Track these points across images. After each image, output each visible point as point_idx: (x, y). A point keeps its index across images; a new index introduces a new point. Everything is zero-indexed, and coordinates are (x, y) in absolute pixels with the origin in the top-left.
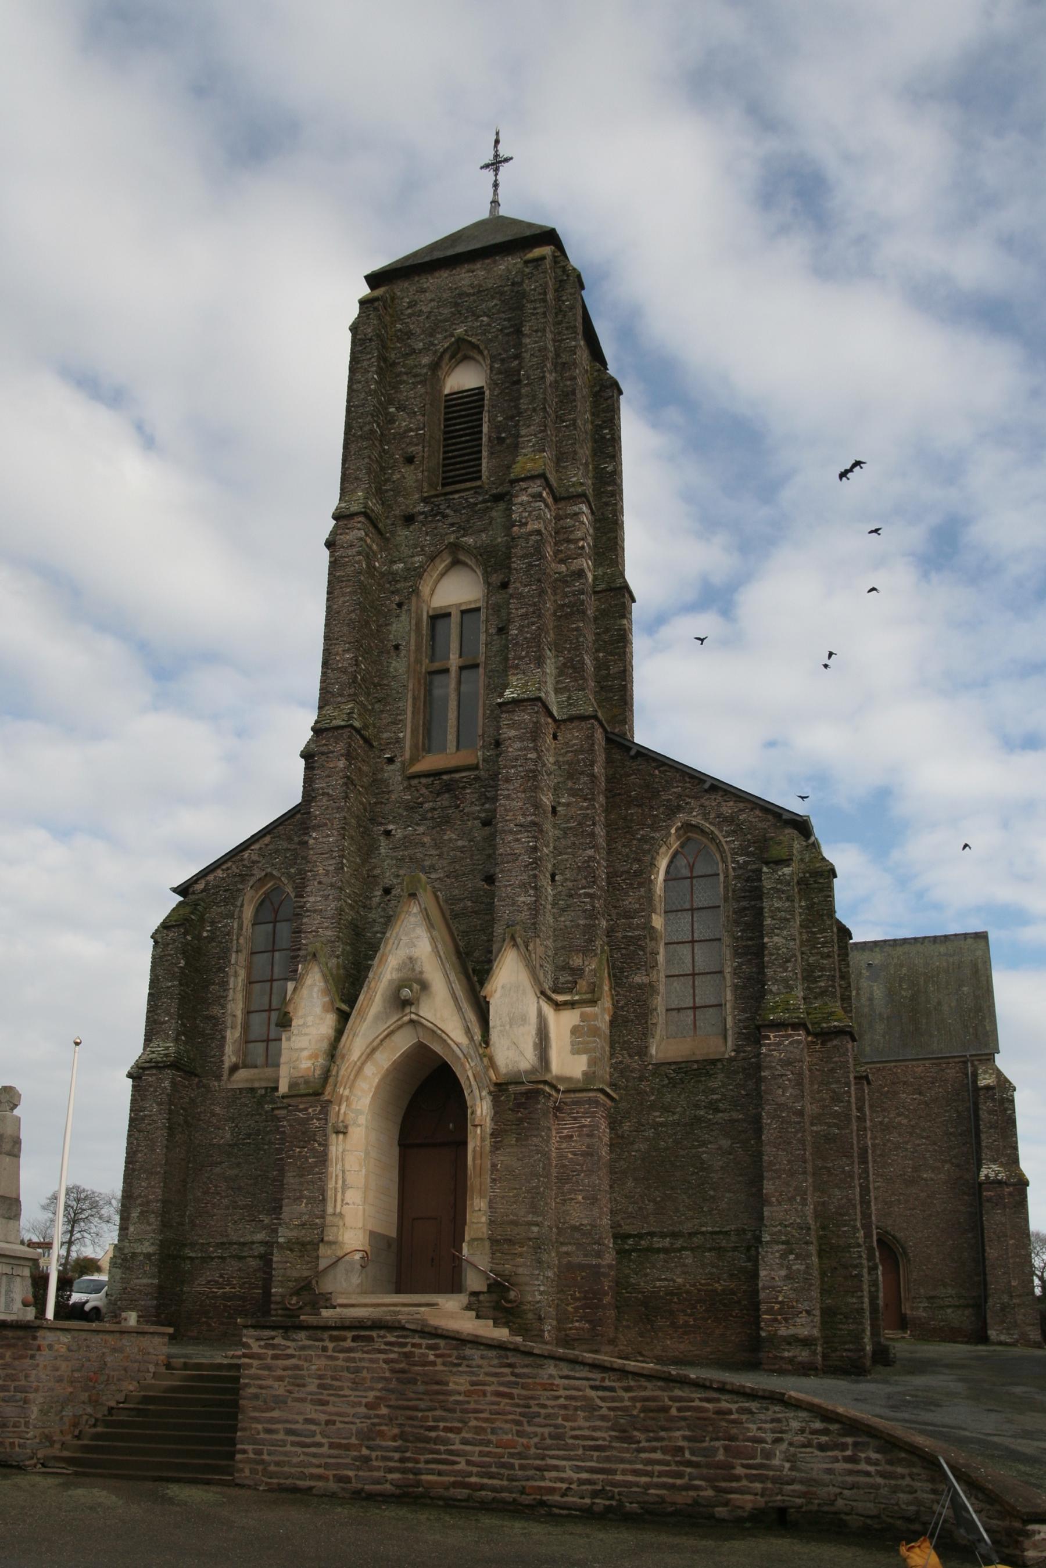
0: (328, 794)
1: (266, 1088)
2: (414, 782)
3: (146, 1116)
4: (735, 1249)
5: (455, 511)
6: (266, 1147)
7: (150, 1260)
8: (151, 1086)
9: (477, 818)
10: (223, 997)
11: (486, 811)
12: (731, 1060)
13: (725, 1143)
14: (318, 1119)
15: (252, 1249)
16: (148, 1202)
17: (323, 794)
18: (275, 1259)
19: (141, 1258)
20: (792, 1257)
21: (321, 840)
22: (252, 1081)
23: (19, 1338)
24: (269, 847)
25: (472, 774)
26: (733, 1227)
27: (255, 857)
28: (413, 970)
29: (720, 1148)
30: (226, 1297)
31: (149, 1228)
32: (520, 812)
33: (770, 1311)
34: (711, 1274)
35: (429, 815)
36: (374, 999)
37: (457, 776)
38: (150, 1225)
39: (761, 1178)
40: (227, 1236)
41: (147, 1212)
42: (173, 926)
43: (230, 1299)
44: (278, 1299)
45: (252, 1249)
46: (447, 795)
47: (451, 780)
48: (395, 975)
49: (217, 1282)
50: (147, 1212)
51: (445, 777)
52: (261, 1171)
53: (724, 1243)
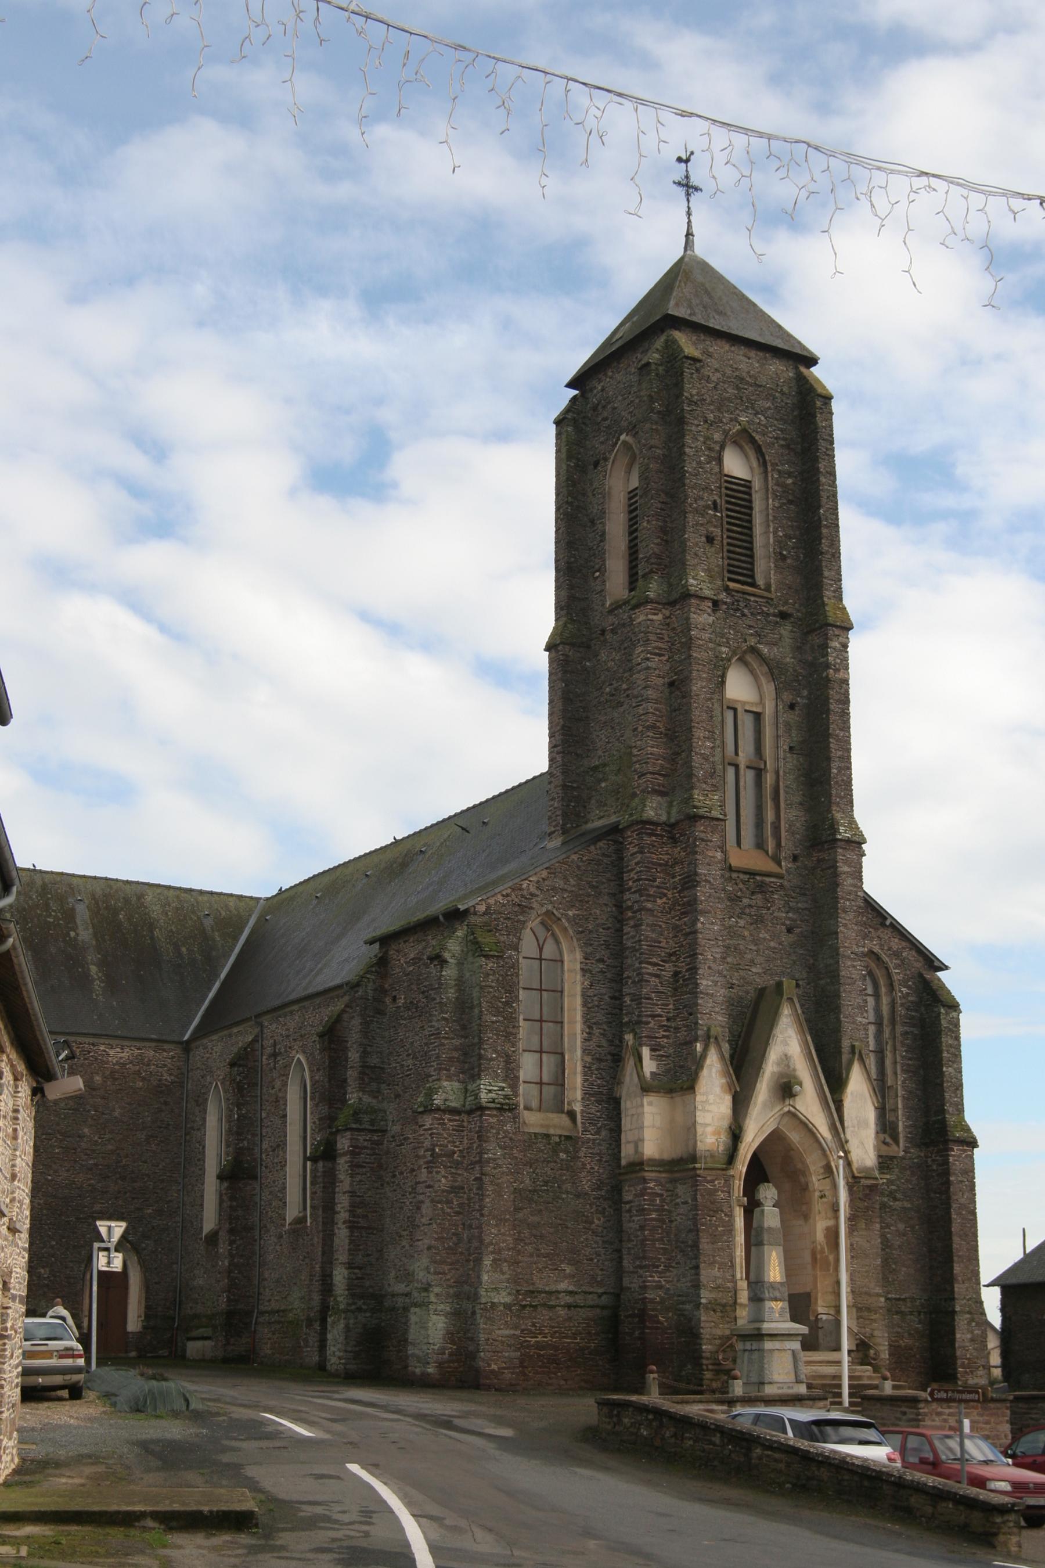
0: (710, 882)
1: (560, 1136)
2: (734, 875)
3: (490, 1158)
4: (911, 1313)
5: (752, 614)
6: (564, 1196)
7: (510, 1310)
8: (492, 1127)
9: (783, 924)
10: (512, 1034)
11: (790, 919)
12: (903, 1158)
13: (901, 1226)
14: (723, 1192)
15: (558, 1298)
16: (499, 1251)
17: (706, 881)
18: (703, 1319)
19: (502, 1308)
20: (974, 1324)
21: (707, 926)
22: (548, 1126)
23: (998, 1409)
24: (546, 883)
25: (778, 881)
26: (907, 1295)
27: (533, 889)
28: (789, 1067)
29: (897, 1231)
30: (539, 1346)
31: (503, 1277)
32: (854, 942)
33: (963, 1366)
34: (897, 1332)
35: (747, 911)
36: (763, 1090)
37: (768, 879)
38: (504, 1274)
39: (952, 1261)
40: (533, 1284)
41: (499, 1260)
42: (493, 956)
43: (543, 1348)
44: (708, 1355)
45: (558, 1298)
46: (760, 896)
47: (762, 882)
48: (776, 1069)
49: (530, 1331)
50: (499, 1260)
51: (758, 878)
52: (561, 1219)
53: (903, 1308)
